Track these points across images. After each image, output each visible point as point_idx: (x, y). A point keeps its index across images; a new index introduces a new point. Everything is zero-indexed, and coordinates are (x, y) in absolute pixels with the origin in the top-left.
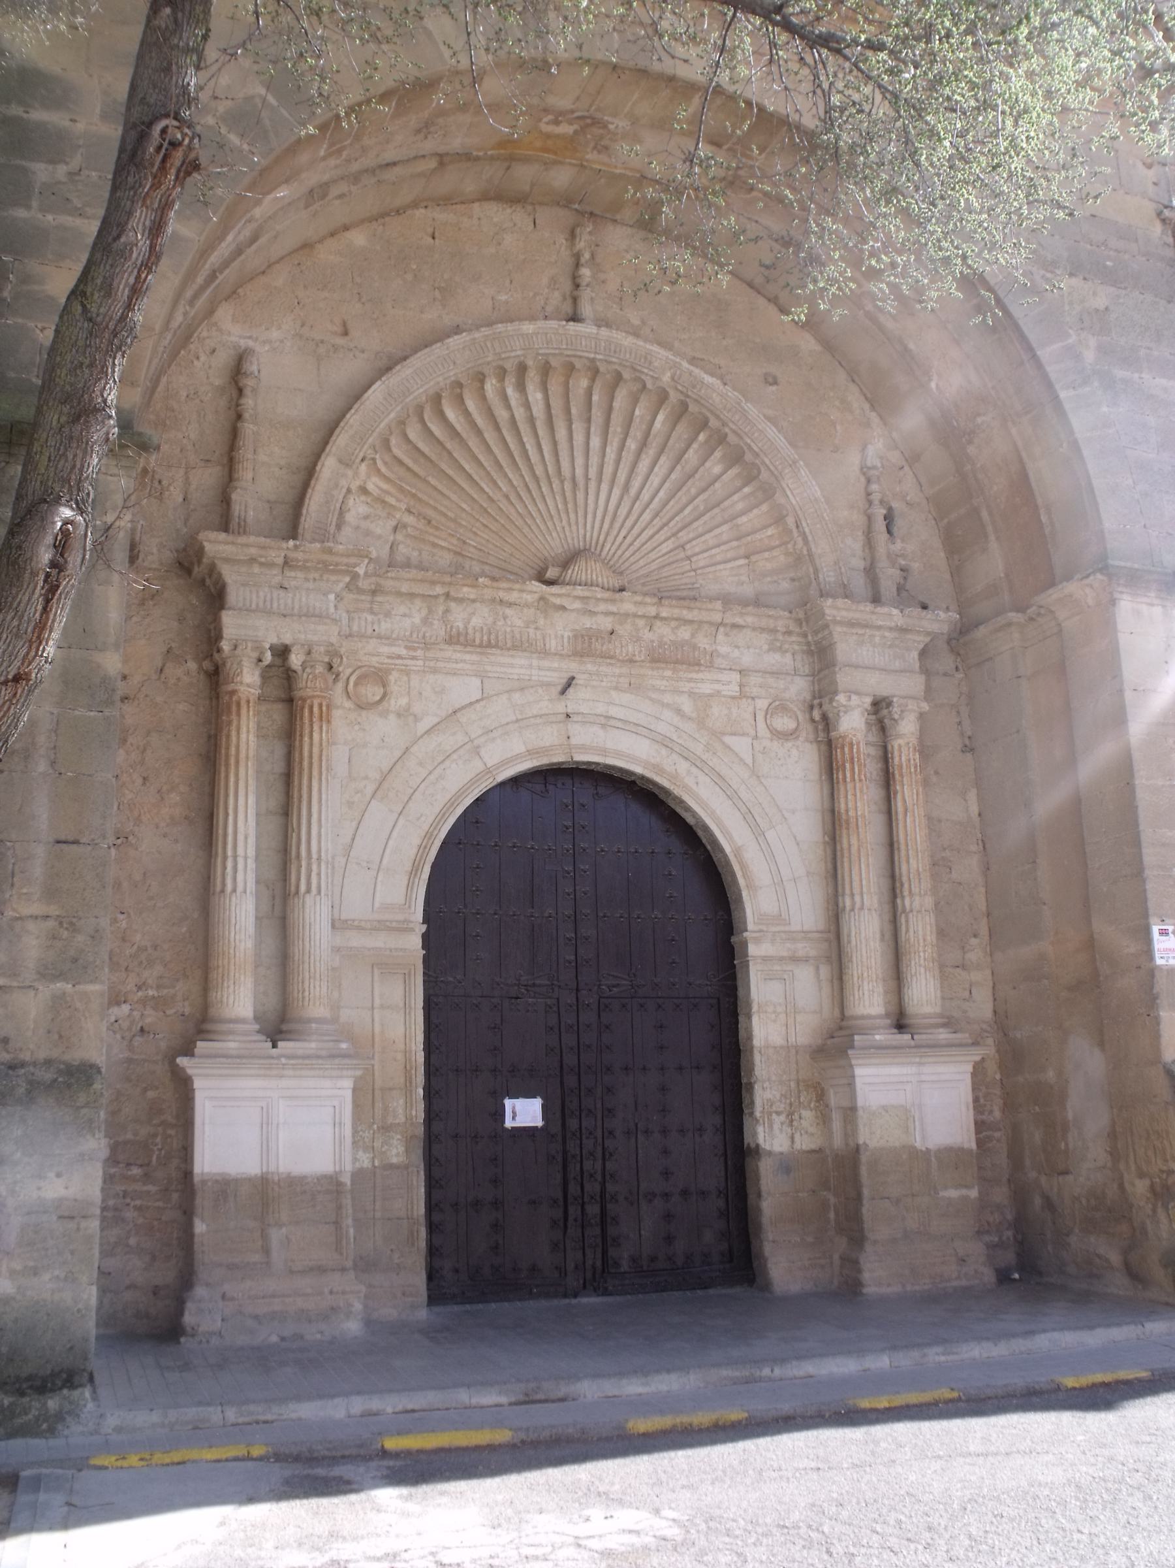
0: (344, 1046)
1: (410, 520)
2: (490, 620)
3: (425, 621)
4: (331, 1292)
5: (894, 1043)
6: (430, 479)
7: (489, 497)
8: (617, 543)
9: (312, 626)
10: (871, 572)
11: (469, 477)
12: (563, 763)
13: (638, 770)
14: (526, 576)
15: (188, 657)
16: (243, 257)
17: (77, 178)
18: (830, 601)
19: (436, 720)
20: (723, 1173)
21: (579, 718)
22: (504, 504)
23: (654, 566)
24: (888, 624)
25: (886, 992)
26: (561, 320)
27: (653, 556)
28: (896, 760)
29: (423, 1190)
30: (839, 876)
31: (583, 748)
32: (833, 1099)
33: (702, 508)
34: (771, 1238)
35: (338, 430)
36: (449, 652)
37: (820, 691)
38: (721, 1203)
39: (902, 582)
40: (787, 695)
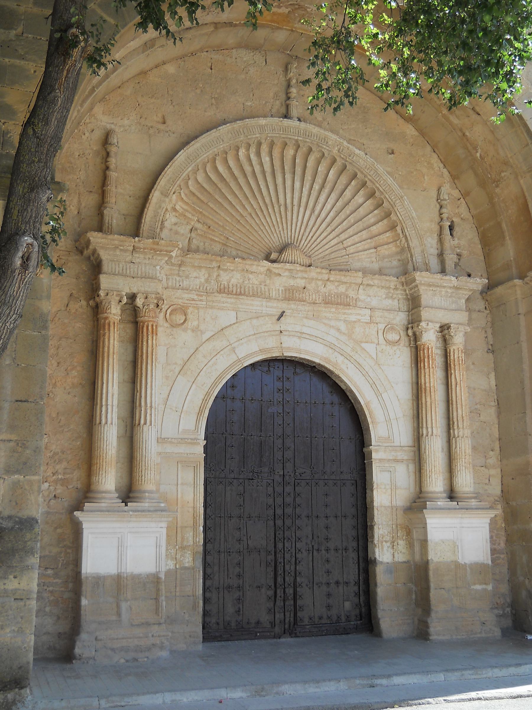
0: (163, 505)
1: (199, 226)
2: (241, 281)
3: (207, 281)
4: (153, 636)
5: (448, 507)
6: (209, 204)
7: (241, 214)
8: (308, 240)
9: (148, 284)
10: (441, 255)
11: (230, 203)
12: (278, 357)
13: (317, 361)
14: (260, 257)
15: (82, 298)
16: (109, 79)
17: (21, 38)
18: (418, 273)
19: (213, 333)
20: (357, 572)
21: (287, 333)
22: (248, 218)
23: (327, 252)
24: (449, 285)
25: (444, 479)
26: (280, 118)
27: (326, 247)
28: (452, 357)
29: (201, 581)
30: (420, 417)
31: (289, 349)
32: (415, 535)
33: (352, 221)
34: (382, 608)
35: (161, 176)
36: (220, 297)
37: (412, 320)
38: (356, 588)
39: (457, 261)
40: (394, 322)
